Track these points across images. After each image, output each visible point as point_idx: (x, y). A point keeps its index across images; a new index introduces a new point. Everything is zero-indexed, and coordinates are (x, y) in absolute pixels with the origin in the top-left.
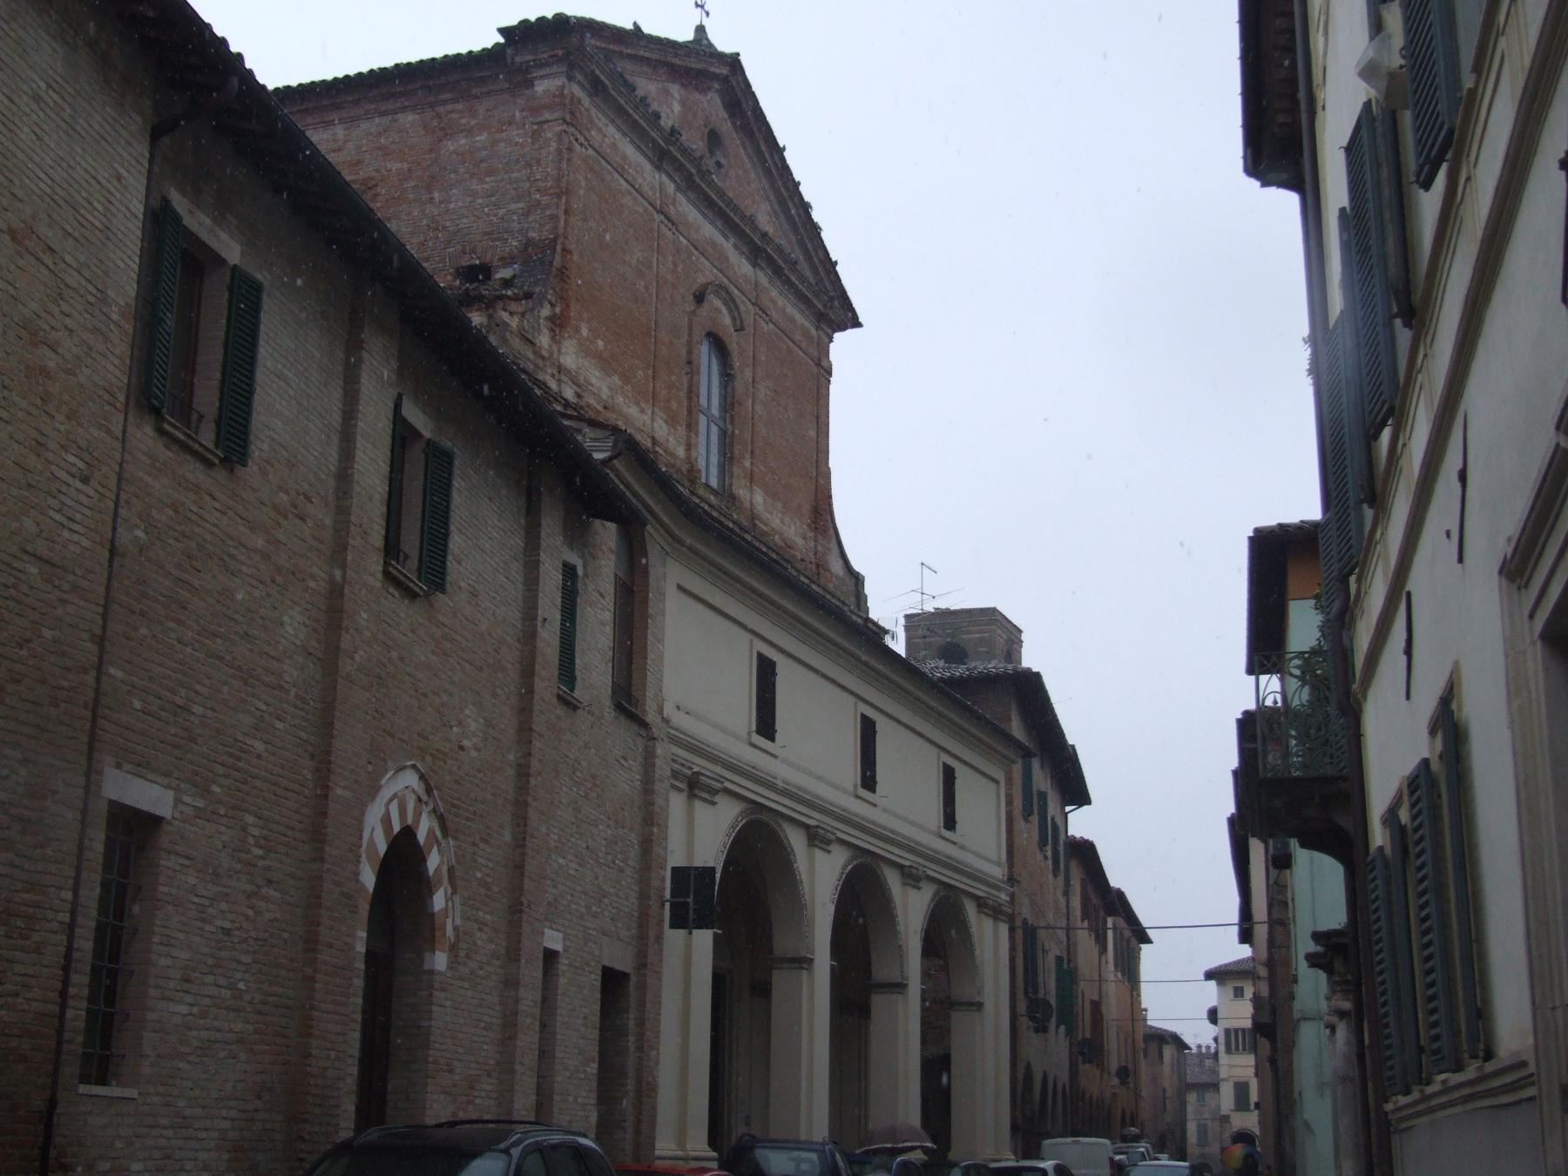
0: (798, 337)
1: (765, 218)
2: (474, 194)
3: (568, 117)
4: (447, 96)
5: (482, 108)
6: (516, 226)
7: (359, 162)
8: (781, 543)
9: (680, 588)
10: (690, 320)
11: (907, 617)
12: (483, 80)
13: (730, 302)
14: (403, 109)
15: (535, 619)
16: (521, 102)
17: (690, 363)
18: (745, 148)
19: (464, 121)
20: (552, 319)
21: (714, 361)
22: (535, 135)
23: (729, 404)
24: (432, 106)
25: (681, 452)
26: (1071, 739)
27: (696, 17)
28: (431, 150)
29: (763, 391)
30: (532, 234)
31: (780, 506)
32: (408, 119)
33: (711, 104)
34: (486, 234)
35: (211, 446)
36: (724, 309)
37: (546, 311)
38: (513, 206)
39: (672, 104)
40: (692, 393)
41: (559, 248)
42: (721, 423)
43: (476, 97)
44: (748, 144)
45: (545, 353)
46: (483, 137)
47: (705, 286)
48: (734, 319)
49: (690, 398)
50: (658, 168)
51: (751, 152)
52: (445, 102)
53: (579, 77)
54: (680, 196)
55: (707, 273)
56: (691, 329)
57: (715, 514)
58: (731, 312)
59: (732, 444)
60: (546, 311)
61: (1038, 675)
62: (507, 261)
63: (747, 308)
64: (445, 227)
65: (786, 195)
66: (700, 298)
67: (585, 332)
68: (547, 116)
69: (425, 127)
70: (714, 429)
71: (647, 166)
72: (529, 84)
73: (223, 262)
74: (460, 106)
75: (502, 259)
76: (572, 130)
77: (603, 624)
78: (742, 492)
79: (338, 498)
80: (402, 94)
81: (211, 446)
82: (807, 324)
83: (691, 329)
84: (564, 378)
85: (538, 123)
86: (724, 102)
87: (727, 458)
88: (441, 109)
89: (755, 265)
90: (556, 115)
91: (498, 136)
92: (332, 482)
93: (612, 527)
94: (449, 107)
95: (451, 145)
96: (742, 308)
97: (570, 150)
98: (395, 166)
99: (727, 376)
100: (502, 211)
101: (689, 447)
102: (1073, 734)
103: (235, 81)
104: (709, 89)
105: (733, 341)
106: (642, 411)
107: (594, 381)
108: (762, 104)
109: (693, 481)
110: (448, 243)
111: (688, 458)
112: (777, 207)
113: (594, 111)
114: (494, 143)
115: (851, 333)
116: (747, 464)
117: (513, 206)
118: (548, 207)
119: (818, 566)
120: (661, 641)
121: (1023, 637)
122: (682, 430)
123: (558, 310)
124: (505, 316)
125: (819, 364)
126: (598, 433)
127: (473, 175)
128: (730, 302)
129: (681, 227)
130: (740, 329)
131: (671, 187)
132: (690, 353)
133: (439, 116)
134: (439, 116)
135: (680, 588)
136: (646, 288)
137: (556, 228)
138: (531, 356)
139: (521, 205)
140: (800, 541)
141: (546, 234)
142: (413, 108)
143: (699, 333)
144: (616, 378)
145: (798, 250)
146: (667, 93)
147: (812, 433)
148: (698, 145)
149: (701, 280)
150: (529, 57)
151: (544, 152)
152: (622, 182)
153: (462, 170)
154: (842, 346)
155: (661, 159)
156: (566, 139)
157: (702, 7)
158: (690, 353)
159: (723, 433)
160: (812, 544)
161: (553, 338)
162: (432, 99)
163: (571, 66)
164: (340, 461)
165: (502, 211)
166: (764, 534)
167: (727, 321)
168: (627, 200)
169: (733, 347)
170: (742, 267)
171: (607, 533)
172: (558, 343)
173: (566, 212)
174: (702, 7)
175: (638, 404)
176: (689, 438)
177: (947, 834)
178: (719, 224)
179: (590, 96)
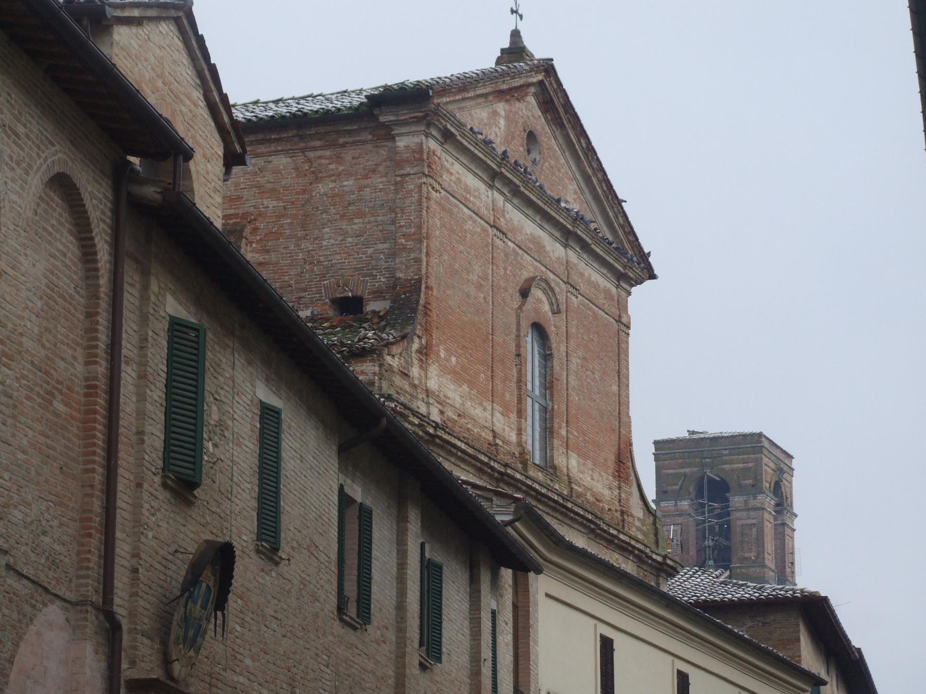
0: (601, 301)
1: (573, 197)
2: (345, 234)
3: (426, 170)
4: (317, 143)
5: (349, 155)
6: (385, 265)
7: (239, 198)
8: (592, 499)
9: (547, 595)
10: (518, 317)
11: (657, 443)
12: (349, 133)
13: (549, 290)
14: (276, 153)
15: (480, 661)
16: (383, 153)
17: (518, 355)
18: (555, 138)
19: (332, 166)
20: (419, 351)
21: (536, 345)
22: (399, 186)
23: (548, 385)
24: (303, 150)
25: (513, 437)
26: (856, 642)
27: (511, 23)
28: (304, 191)
29: (575, 362)
30: (400, 275)
31: (589, 464)
32: (282, 161)
33: (529, 108)
34: (356, 269)
35: (354, 616)
36: (544, 299)
37: (415, 346)
38: (381, 246)
39: (494, 122)
40: (520, 382)
41: (423, 286)
42: (542, 402)
43: (343, 146)
44: (558, 133)
45: (416, 382)
46: (349, 183)
47: (530, 281)
48: (551, 304)
49: (519, 388)
50: (491, 187)
51: (561, 140)
52: (314, 149)
53: (434, 133)
54: (509, 206)
55: (529, 268)
56: (518, 324)
57: (544, 491)
58: (549, 298)
59: (552, 419)
60: (415, 346)
61: (825, 599)
62: (378, 294)
63: (561, 288)
64: (319, 262)
65: (590, 171)
66: (524, 293)
67: (442, 354)
68: (408, 170)
69: (296, 169)
70: (537, 406)
71: (482, 187)
72: (393, 138)
73: (354, 501)
74: (328, 153)
75: (373, 292)
76: (430, 180)
77: (507, 645)
78: (560, 460)
79: (397, 622)
80: (276, 140)
81: (354, 616)
82: (609, 285)
83: (518, 324)
84: (431, 401)
85: (401, 176)
86: (539, 103)
87: (548, 431)
88: (311, 154)
89: (566, 246)
90: (415, 170)
91: (365, 182)
92: (394, 612)
93: (510, 571)
94: (318, 153)
95: (321, 188)
96: (557, 289)
97: (428, 199)
98: (271, 204)
99: (547, 357)
100: (370, 251)
101: (520, 432)
102: (856, 639)
103: (384, 421)
104: (526, 95)
105: (553, 325)
106: (485, 409)
107: (450, 394)
108: (571, 98)
109: (525, 463)
110: (323, 276)
111: (520, 444)
112: (583, 185)
113: (444, 156)
114: (361, 189)
115: (649, 283)
116: (563, 432)
117: (381, 246)
118: (411, 250)
119: (622, 513)
120: (536, 643)
121: (795, 464)
122: (513, 416)
123: (424, 341)
124: (388, 359)
125: (619, 321)
126: (503, 502)
127: (342, 217)
128: (549, 290)
129: (510, 235)
130: (556, 312)
131: (500, 199)
132: (518, 346)
133: (309, 161)
134: (309, 161)
135: (547, 595)
136: (485, 298)
137: (420, 269)
138: (407, 388)
139: (386, 245)
140: (606, 492)
141: (411, 274)
142: (285, 152)
143: (525, 325)
144: (465, 387)
145: (600, 219)
146: (495, 113)
147: (615, 388)
148: (517, 151)
149: (526, 275)
150: (392, 118)
151: (407, 202)
152: (466, 210)
153: (333, 211)
154: (641, 300)
155: (493, 179)
156: (424, 189)
157: (516, 12)
158: (518, 346)
159: (544, 409)
160: (616, 492)
161: (421, 367)
162: (302, 145)
163: (428, 125)
164: (397, 597)
165: (370, 251)
166: (579, 495)
167: (546, 307)
168: (469, 226)
169: (551, 330)
170: (555, 249)
171: (507, 574)
172: (426, 370)
173: (427, 254)
174: (516, 12)
175: (481, 404)
176: (519, 423)
177: (685, 668)
178: (538, 218)
179: (442, 144)
